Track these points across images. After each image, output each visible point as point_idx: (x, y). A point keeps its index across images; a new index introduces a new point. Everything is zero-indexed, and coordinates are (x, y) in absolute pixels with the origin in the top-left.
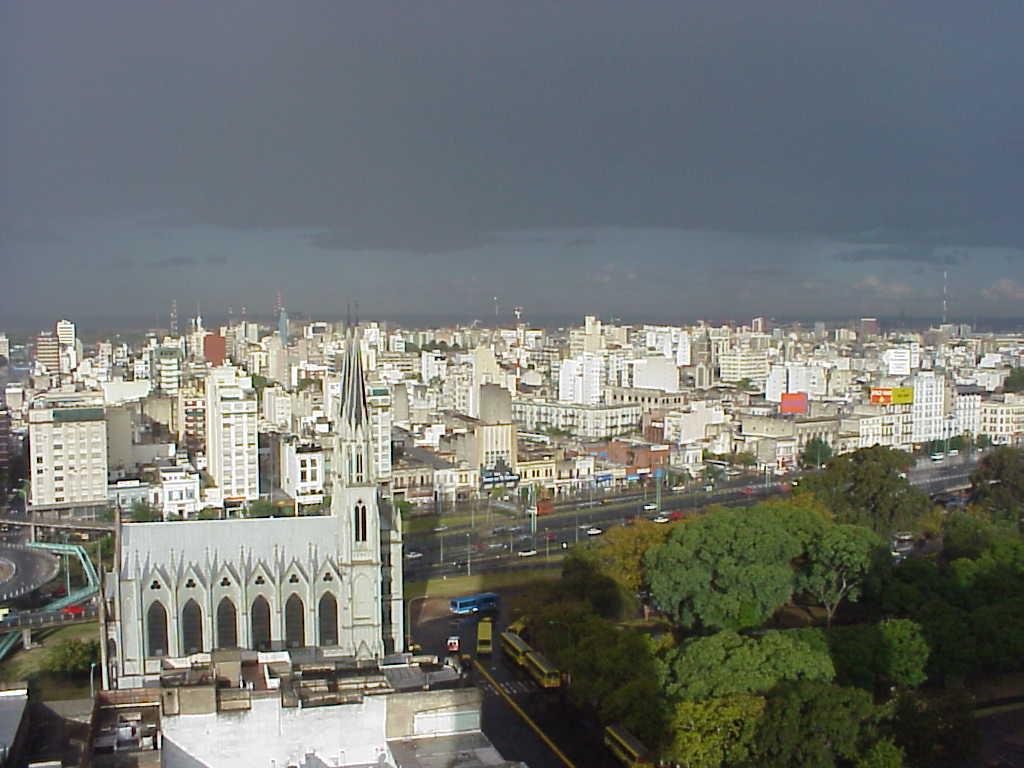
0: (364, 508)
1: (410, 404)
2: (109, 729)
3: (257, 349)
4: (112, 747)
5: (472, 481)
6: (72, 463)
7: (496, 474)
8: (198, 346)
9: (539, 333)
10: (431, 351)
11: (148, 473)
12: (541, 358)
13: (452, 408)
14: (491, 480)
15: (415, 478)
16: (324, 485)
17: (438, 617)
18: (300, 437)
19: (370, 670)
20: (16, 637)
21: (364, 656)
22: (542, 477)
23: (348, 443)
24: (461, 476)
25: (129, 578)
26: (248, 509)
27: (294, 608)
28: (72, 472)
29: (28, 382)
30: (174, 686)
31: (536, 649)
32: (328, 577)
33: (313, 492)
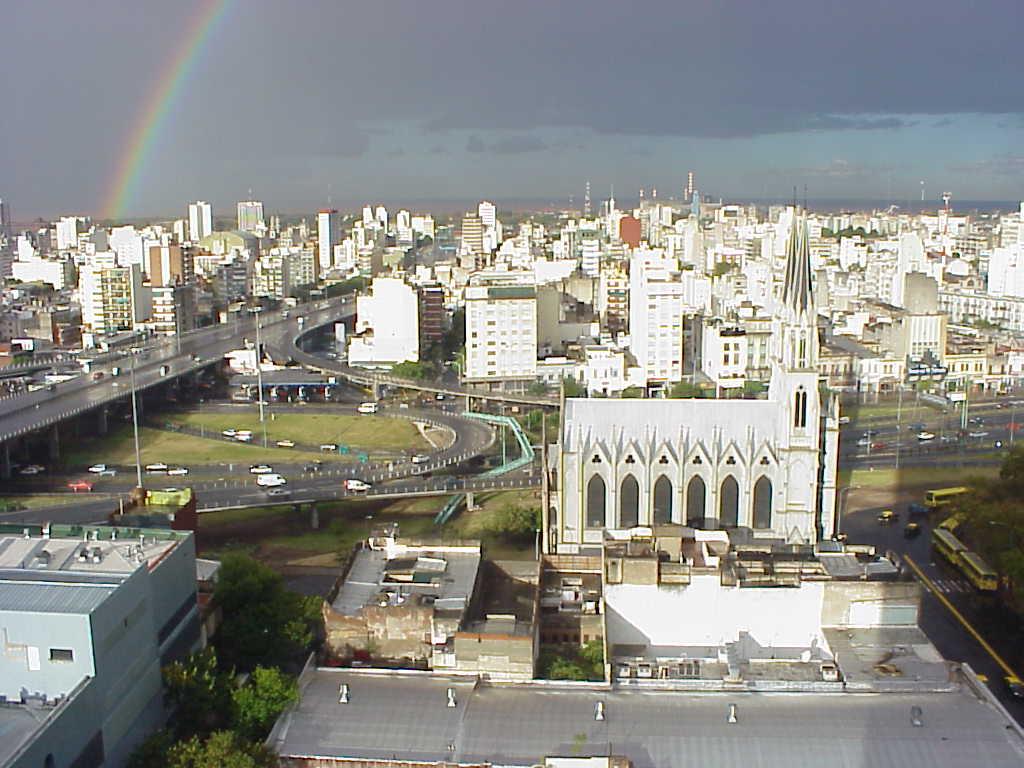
0: (805, 394)
1: (830, 290)
2: (554, 591)
3: (672, 231)
4: (557, 608)
5: (897, 371)
6: (504, 339)
7: (922, 366)
8: (614, 228)
9: (962, 220)
10: (850, 237)
11: (573, 350)
12: (965, 247)
13: (874, 296)
14: (917, 371)
15: (838, 366)
16: (747, 369)
17: (865, 508)
18: (724, 320)
19: (805, 555)
20: (461, 498)
21: (796, 539)
22: (971, 371)
23: (792, 328)
24: (885, 366)
25: (571, 450)
26: (670, 390)
27: (730, 489)
28: (504, 347)
29: (455, 260)
30: (618, 557)
31: (971, 549)
32: (765, 461)
33: (735, 376)
